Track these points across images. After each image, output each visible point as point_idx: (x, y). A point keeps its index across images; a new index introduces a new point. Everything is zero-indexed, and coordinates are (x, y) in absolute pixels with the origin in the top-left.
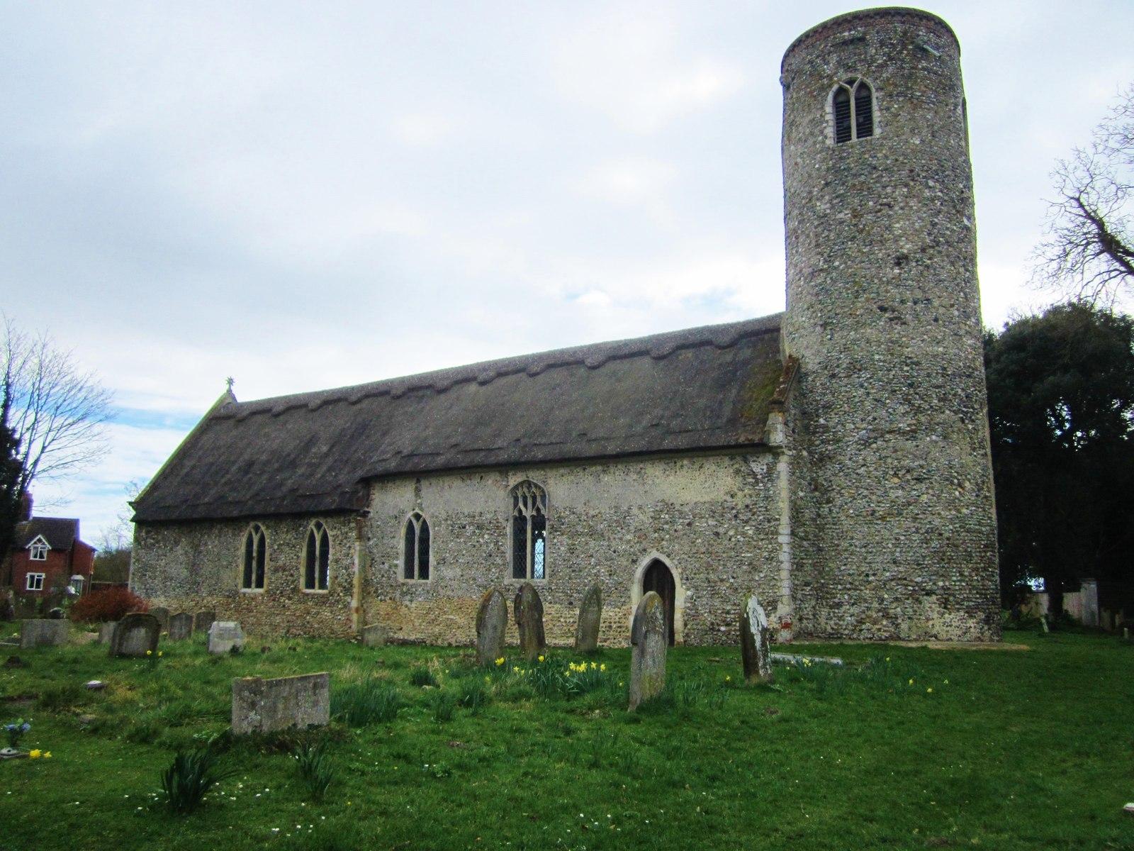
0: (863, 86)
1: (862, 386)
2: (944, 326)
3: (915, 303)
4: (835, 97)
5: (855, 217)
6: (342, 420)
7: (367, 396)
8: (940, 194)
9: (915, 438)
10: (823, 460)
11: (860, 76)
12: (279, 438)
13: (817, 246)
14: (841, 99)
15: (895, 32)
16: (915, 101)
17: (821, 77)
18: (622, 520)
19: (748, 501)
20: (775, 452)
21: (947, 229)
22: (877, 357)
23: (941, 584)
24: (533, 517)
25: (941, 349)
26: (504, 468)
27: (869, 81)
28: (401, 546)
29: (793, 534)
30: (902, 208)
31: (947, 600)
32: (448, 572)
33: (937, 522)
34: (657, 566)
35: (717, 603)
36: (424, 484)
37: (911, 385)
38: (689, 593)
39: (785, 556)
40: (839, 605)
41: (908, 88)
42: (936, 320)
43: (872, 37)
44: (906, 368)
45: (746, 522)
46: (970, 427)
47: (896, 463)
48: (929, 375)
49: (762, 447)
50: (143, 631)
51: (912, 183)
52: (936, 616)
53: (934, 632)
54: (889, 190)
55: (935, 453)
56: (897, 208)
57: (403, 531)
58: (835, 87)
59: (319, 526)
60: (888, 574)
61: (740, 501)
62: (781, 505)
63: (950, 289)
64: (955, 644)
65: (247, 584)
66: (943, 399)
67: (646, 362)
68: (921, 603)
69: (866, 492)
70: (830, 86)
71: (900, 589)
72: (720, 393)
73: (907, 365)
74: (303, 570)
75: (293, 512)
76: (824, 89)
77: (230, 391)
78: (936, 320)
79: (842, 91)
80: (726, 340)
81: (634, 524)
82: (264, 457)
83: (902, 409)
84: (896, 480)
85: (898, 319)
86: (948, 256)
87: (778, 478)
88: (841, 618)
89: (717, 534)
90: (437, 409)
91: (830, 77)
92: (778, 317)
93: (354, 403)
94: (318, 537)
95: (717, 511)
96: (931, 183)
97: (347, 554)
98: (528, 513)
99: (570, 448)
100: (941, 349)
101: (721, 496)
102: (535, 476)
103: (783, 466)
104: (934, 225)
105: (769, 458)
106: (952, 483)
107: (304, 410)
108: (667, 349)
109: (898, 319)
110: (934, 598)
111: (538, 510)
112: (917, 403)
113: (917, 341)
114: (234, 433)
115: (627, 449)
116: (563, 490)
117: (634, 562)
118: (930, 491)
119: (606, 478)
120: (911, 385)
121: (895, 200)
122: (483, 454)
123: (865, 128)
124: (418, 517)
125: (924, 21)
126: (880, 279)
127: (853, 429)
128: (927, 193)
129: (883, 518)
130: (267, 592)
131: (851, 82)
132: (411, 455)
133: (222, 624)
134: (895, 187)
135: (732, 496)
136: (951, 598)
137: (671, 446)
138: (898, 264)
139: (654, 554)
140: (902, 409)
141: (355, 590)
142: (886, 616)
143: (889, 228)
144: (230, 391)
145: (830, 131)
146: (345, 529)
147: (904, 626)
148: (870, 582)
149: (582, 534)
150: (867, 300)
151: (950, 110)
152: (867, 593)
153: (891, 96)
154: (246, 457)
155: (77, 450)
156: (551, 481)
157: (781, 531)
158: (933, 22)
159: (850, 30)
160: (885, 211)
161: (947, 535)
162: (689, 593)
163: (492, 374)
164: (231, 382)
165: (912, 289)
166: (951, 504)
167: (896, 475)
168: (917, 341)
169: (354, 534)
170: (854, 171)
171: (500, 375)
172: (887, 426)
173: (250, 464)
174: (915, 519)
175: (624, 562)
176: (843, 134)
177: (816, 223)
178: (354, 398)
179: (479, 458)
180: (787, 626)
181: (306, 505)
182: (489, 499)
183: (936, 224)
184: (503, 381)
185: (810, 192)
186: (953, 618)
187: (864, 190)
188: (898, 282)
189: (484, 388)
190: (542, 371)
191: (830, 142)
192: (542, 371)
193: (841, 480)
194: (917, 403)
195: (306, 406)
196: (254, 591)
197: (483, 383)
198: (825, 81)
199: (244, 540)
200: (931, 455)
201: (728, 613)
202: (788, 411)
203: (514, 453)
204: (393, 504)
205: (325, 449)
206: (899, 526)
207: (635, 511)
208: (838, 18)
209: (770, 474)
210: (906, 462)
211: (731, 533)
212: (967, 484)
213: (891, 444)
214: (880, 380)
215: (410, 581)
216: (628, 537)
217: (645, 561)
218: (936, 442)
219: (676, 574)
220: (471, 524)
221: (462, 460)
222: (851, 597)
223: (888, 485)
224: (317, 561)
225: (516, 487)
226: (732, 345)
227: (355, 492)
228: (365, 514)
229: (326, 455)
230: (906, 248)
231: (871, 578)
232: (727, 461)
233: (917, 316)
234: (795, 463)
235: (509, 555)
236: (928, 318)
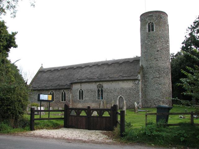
0: (152, 23)
10: (146, 81)
19: (135, 88)
20: (139, 80)
26: (96, 82)
28: (78, 94)
40: (148, 103)
57: (78, 92)
58: (148, 23)
61: (134, 87)
77: (42, 66)
102: (101, 83)
103: (140, 82)
105: (138, 81)
116: (106, 86)
119: (113, 84)
123: (153, 30)
124: (81, 90)
131: (151, 22)
142: (155, 104)
144: (42, 66)
164: (42, 64)
169: (70, 92)
176: (149, 31)
203: (97, 80)
209: (138, 84)
210: (158, 82)
232: (132, 81)
234: (142, 82)
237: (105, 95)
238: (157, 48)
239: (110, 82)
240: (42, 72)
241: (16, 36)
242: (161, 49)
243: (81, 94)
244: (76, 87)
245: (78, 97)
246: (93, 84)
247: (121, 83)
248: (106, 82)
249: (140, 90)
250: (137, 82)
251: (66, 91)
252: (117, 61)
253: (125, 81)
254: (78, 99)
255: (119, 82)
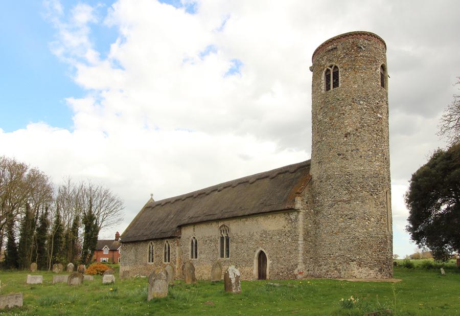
0: (336, 67)
1: (330, 184)
2: (365, 159)
3: (352, 151)
4: (326, 73)
5: (330, 120)
6: (179, 206)
7: (187, 198)
8: (366, 106)
9: (350, 203)
10: (317, 213)
11: (334, 63)
12: (161, 213)
13: (318, 132)
14: (328, 74)
15: (349, 43)
16: (356, 70)
17: (321, 66)
18: (251, 237)
19: (289, 229)
20: (298, 211)
21: (368, 120)
22: (336, 173)
23: (358, 257)
24: (226, 237)
25: (362, 168)
26: (218, 220)
27: (337, 65)
28: (190, 247)
29: (304, 240)
30: (348, 114)
31: (361, 263)
32: (203, 256)
33: (357, 234)
34: (261, 253)
35: (279, 265)
36: (196, 227)
37: (349, 183)
38: (271, 262)
39: (300, 248)
40: (321, 265)
41: (353, 65)
42: (361, 157)
43: (340, 47)
44: (347, 177)
45: (289, 236)
46: (375, 197)
47: (341, 213)
48: (356, 179)
49: (292, 210)
50: (78, 278)
51: (353, 104)
52: (355, 269)
53: (355, 275)
54: (343, 108)
55: (358, 208)
56: (346, 115)
57: (190, 243)
58: (325, 69)
59: (167, 242)
60: (337, 254)
61: (287, 229)
62: (299, 230)
63: (368, 144)
64: (363, 280)
65: (150, 262)
66: (362, 187)
67: (267, 180)
68: (349, 264)
69: (331, 224)
70: (324, 69)
71: (342, 260)
72: (282, 190)
73: (348, 175)
74: (163, 256)
75: (160, 239)
76: (322, 70)
77: (152, 198)
78: (361, 157)
79: (328, 70)
80: (292, 170)
81: (255, 238)
82: (156, 220)
83: (345, 192)
84: (342, 219)
85: (345, 158)
86: (368, 131)
87: (299, 220)
88: (321, 270)
89: (280, 241)
90: (207, 201)
91: (324, 65)
92: (309, 161)
93: (183, 200)
94: (151, 246)
95: (280, 233)
96: (361, 102)
97: (175, 251)
98: (224, 235)
99: (235, 213)
100: (362, 168)
101: (282, 228)
102: (226, 223)
103: (301, 216)
104: (362, 119)
105: (296, 213)
106: (365, 219)
107: (170, 204)
108: (274, 175)
109: (345, 158)
110: (355, 262)
111: (227, 235)
112: (351, 190)
113: (352, 166)
114: (151, 212)
115: (252, 213)
116: (235, 228)
117: (255, 251)
118: (355, 223)
119: (247, 223)
120: (349, 183)
121: (346, 111)
122: (211, 216)
123: (336, 85)
124: (194, 238)
125: (363, 35)
126: (339, 143)
127: (328, 201)
128: (360, 107)
129: (336, 234)
130: (155, 263)
131: (331, 67)
132: (192, 217)
133: (107, 276)
134: (346, 106)
135: (285, 228)
136: (362, 263)
137: (264, 211)
138: (346, 136)
139: (261, 249)
140: (345, 192)
141: (177, 262)
142: (336, 269)
143: (343, 123)
144: (152, 198)
145: (323, 87)
146: (174, 243)
147: (343, 273)
148: (331, 257)
149: (239, 243)
150: (334, 152)
151: (373, 71)
152: (330, 261)
153: (346, 69)
154: (152, 220)
155: (113, 220)
156: (231, 225)
157: (299, 239)
158: (367, 35)
159: (331, 45)
160: (342, 116)
161: (361, 239)
162: (271, 262)
163: (222, 188)
164: (152, 195)
165: (351, 145)
166: (364, 227)
167: (341, 217)
168: (352, 166)
169: (176, 244)
170: (331, 102)
171: (225, 188)
172: (338, 199)
173: (153, 222)
174: (348, 234)
175: (252, 251)
176: (328, 88)
177: (318, 124)
178: (183, 199)
179: (209, 218)
180: (300, 273)
181: (164, 235)
182: (212, 231)
183: (363, 118)
184: (225, 189)
185: (316, 112)
186: (363, 270)
187: (333, 109)
188: (345, 144)
189: (220, 192)
190: (237, 186)
191: (323, 92)
192: (237, 186)
193: (322, 220)
194: (351, 190)
195: (170, 202)
196: (151, 263)
197: (219, 191)
198: (322, 67)
199: (148, 247)
200: (356, 209)
201: (283, 268)
202: (304, 195)
203: (219, 216)
204: (187, 233)
205: (172, 216)
206: (342, 236)
207: (255, 234)
208: (327, 41)
209: (296, 219)
210: (345, 212)
211: (284, 240)
212: (372, 219)
213: (340, 206)
214: (337, 182)
215: (192, 259)
216: (253, 243)
217: (258, 251)
218: (358, 204)
219: (267, 255)
220: (209, 240)
221: (205, 218)
222: (324, 263)
223: (338, 221)
224: (168, 254)
225: (221, 227)
226: (295, 172)
227: (176, 231)
228: (180, 238)
229: (172, 218)
230: (349, 130)
231: (331, 256)
232: (283, 215)
233: (352, 156)
234: (306, 215)
235: (219, 250)
236: (357, 156)
237: (232, 246)
238: (346, 127)
239: (242, 220)
240: (151, 207)
241: (65, 132)
242: (357, 130)
243: (195, 245)
244: (187, 233)
245: (190, 253)
246: (214, 225)
247: (261, 219)
248: (234, 221)
249: (301, 235)
250: (293, 216)
251: (171, 243)
252: (259, 176)
253: (270, 216)
254: (190, 259)
255: (259, 217)
